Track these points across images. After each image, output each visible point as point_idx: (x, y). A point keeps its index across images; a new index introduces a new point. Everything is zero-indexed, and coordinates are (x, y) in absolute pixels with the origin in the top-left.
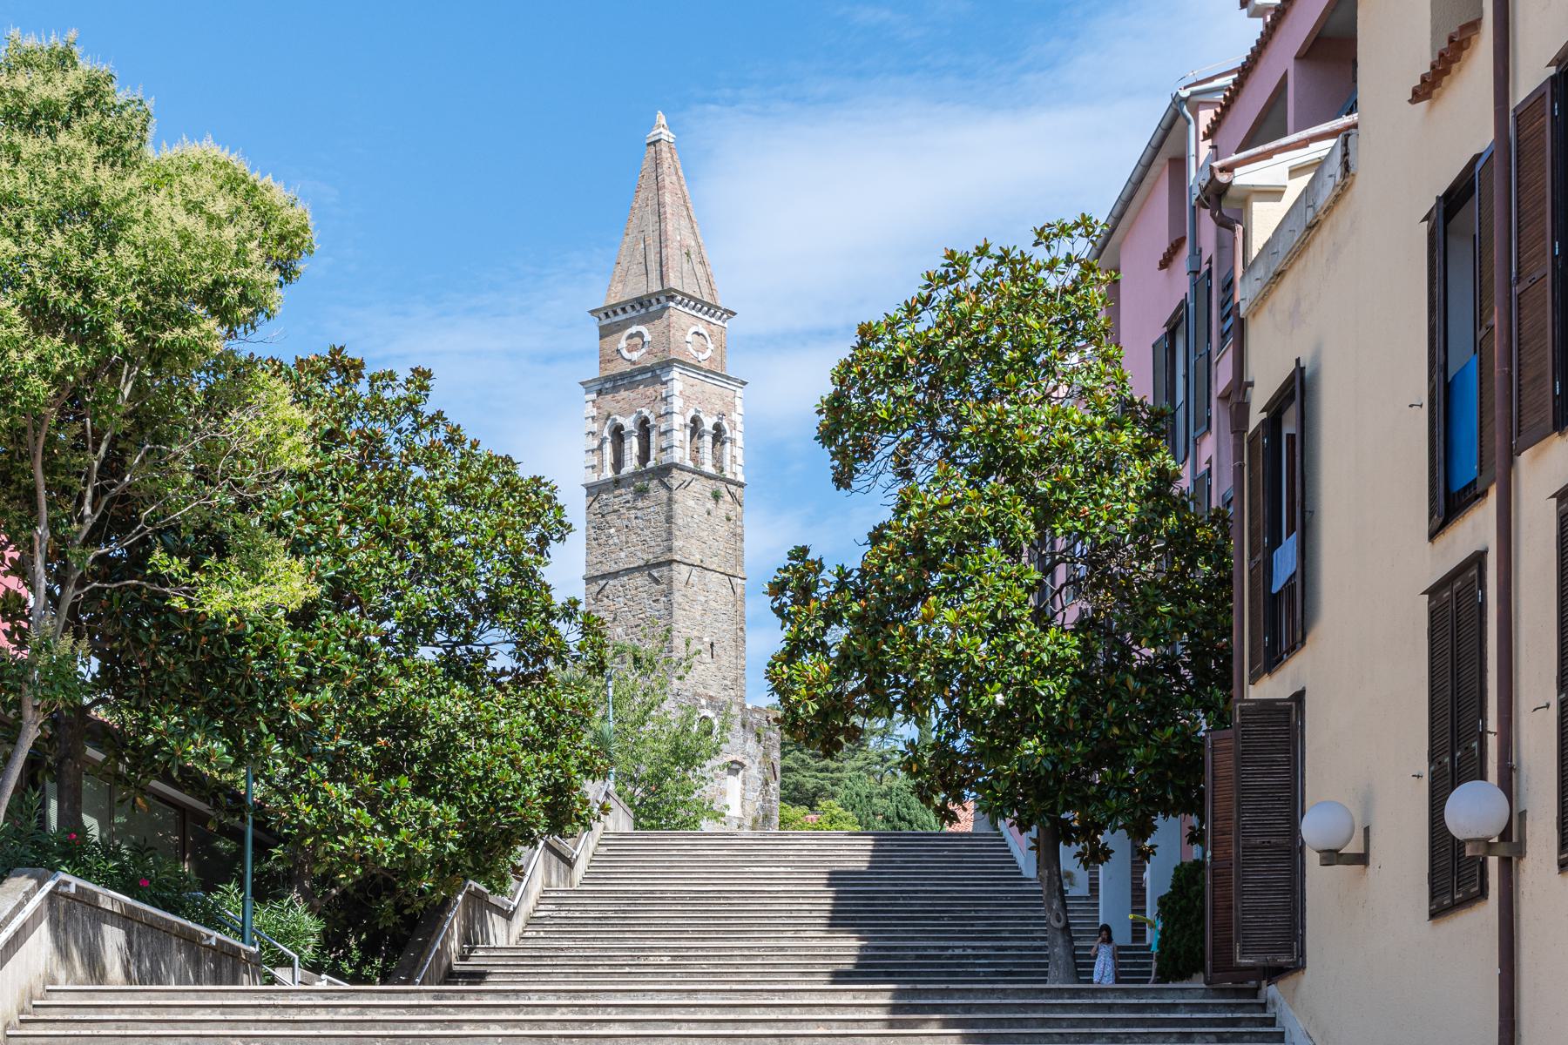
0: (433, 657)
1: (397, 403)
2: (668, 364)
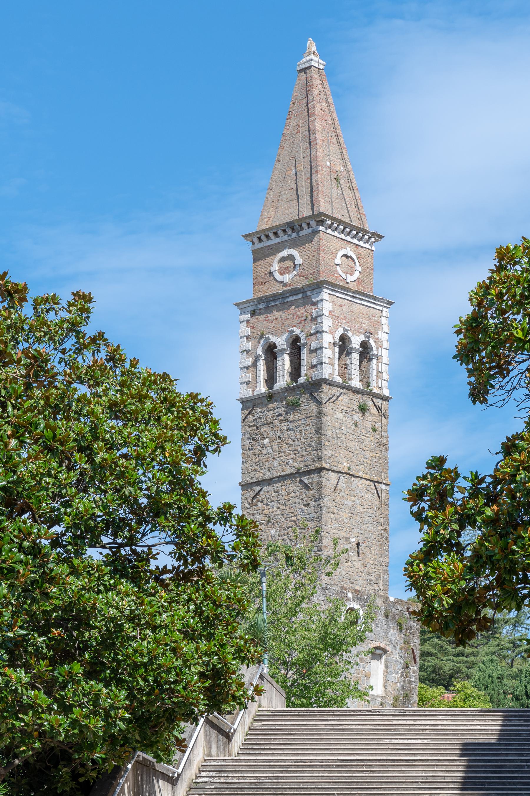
0: (100, 557)
1: (60, 325)
2: (318, 286)
